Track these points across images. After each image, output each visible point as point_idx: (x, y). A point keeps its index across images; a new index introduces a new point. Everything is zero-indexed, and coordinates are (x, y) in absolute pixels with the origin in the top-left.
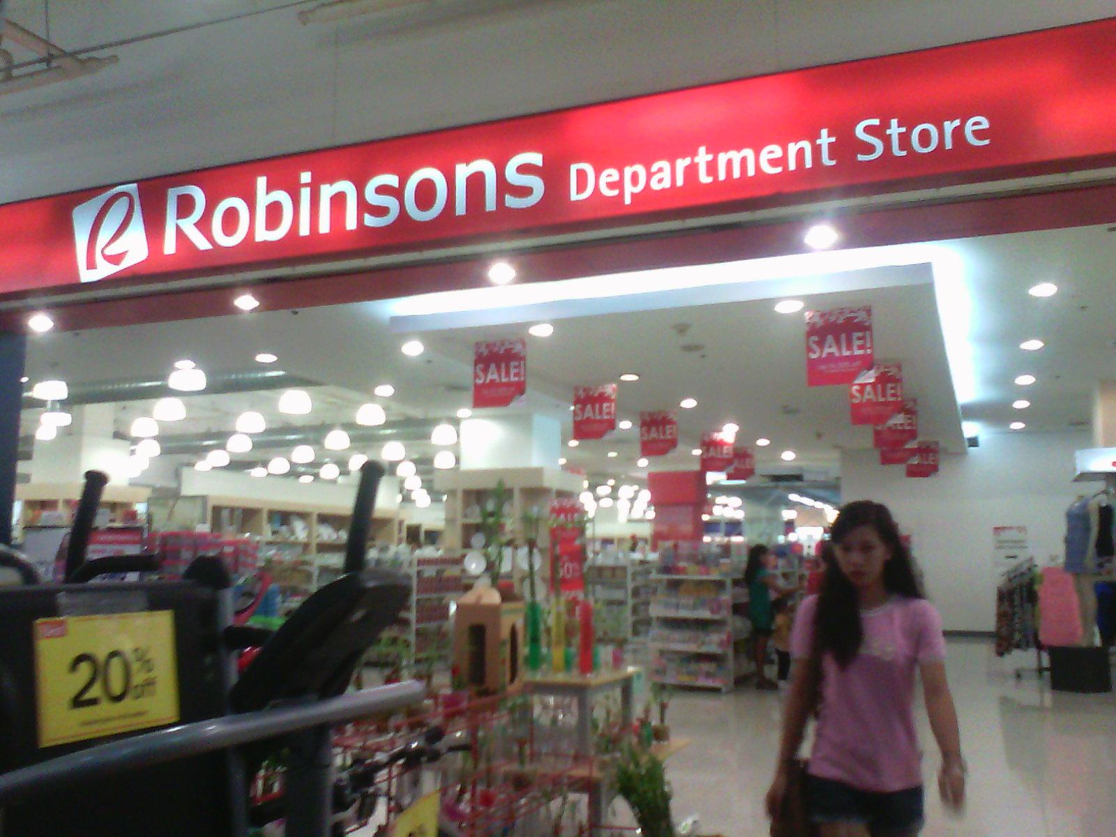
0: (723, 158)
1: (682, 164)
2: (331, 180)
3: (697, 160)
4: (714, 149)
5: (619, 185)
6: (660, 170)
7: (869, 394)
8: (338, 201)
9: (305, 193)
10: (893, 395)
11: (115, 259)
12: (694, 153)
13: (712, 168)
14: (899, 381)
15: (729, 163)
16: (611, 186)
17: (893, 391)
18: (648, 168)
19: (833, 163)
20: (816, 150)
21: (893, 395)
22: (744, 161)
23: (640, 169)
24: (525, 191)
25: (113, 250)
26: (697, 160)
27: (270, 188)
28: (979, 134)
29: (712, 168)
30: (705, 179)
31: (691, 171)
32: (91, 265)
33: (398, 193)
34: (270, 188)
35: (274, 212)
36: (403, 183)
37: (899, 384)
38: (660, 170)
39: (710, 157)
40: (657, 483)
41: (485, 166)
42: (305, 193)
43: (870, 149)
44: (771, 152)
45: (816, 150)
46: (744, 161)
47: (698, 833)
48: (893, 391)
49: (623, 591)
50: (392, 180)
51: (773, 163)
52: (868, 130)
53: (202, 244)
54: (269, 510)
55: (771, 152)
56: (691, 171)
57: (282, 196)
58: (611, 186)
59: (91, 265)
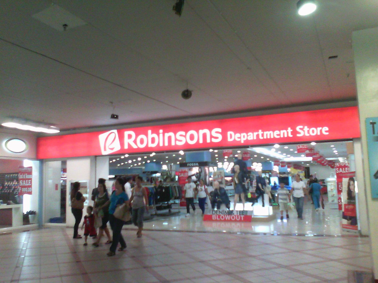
0: (265, 133)
1: (255, 134)
2: (168, 132)
3: (259, 133)
4: (263, 131)
5: (240, 138)
6: (250, 135)
7: (341, 171)
8: (170, 138)
9: (161, 135)
10: (347, 171)
11: (112, 149)
12: (258, 132)
13: (263, 135)
14: (349, 167)
15: (267, 135)
16: (238, 138)
17: (347, 170)
18: (247, 134)
19: (292, 136)
20: (288, 132)
21: (347, 171)
22: (270, 134)
23: (245, 134)
24: (216, 138)
25: (111, 147)
26: (259, 133)
27: (152, 133)
28: (326, 131)
29: (263, 135)
30: (261, 138)
31: (258, 136)
32: (105, 150)
33: (185, 136)
34: (152, 133)
35: (153, 140)
36: (186, 134)
37: (349, 168)
38: (250, 135)
39: (262, 133)
40: (337, 174)
41: (206, 131)
42: (161, 135)
43: (299, 133)
44: (277, 132)
45: (288, 132)
46: (270, 134)
47: (195, 205)
48: (347, 170)
49: (108, 179)
50: (183, 133)
51: (278, 135)
52: (300, 129)
53: (135, 147)
54: (57, 190)
55: (277, 132)
56: (258, 136)
57: (155, 135)
58: (238, 138)
59: (105, 150)
